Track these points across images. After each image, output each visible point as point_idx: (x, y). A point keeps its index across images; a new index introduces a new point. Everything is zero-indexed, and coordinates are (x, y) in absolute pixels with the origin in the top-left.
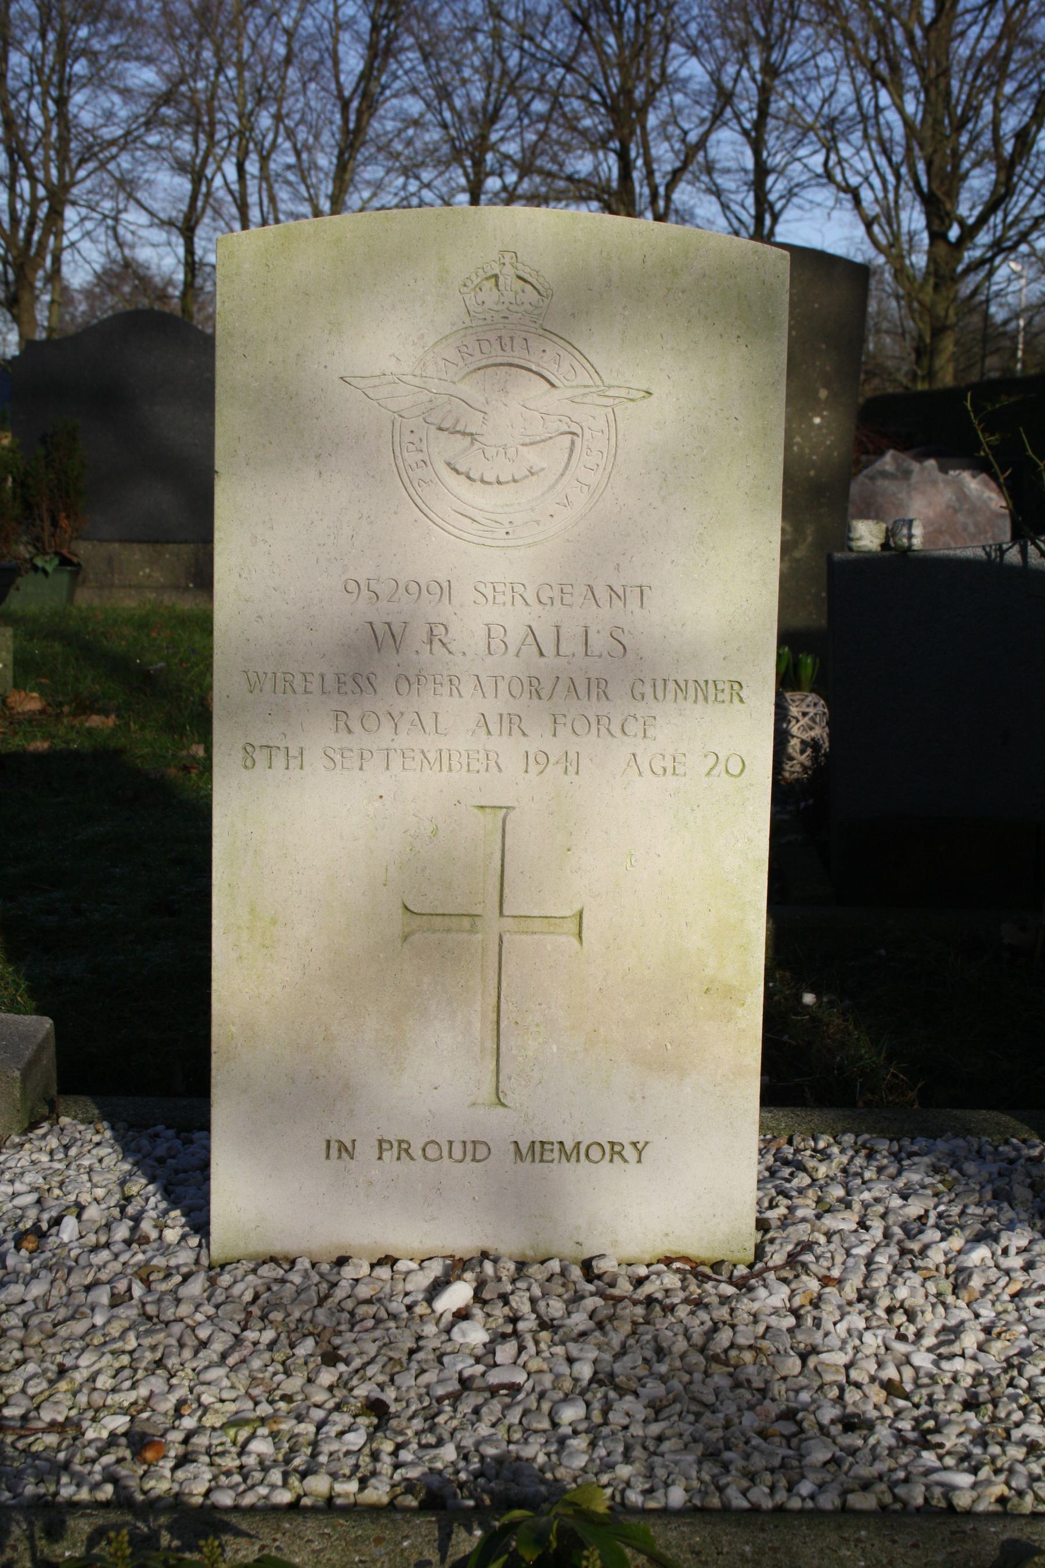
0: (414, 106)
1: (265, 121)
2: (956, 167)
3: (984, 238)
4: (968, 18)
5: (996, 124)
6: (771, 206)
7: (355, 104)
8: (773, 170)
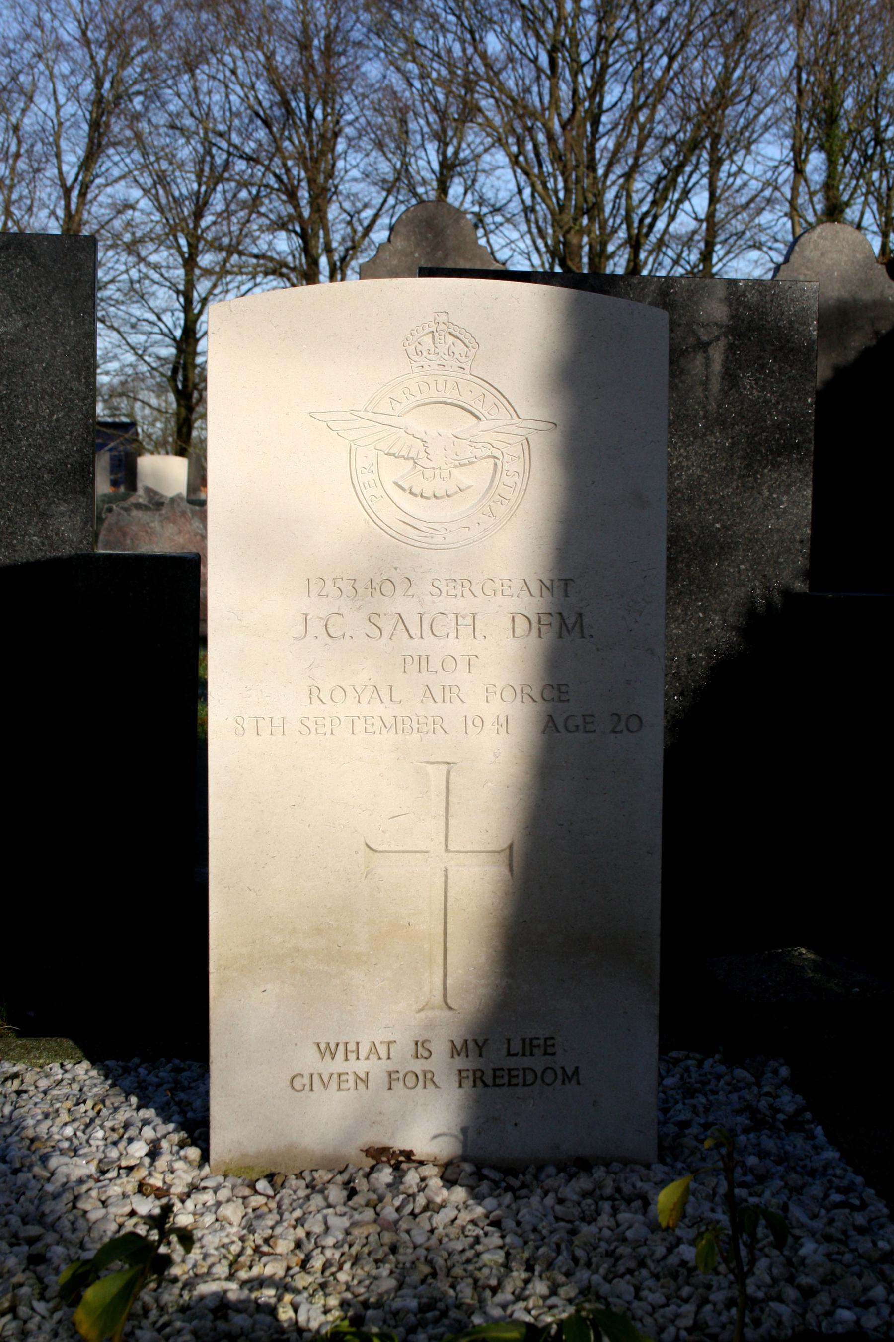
7: (75, 193)
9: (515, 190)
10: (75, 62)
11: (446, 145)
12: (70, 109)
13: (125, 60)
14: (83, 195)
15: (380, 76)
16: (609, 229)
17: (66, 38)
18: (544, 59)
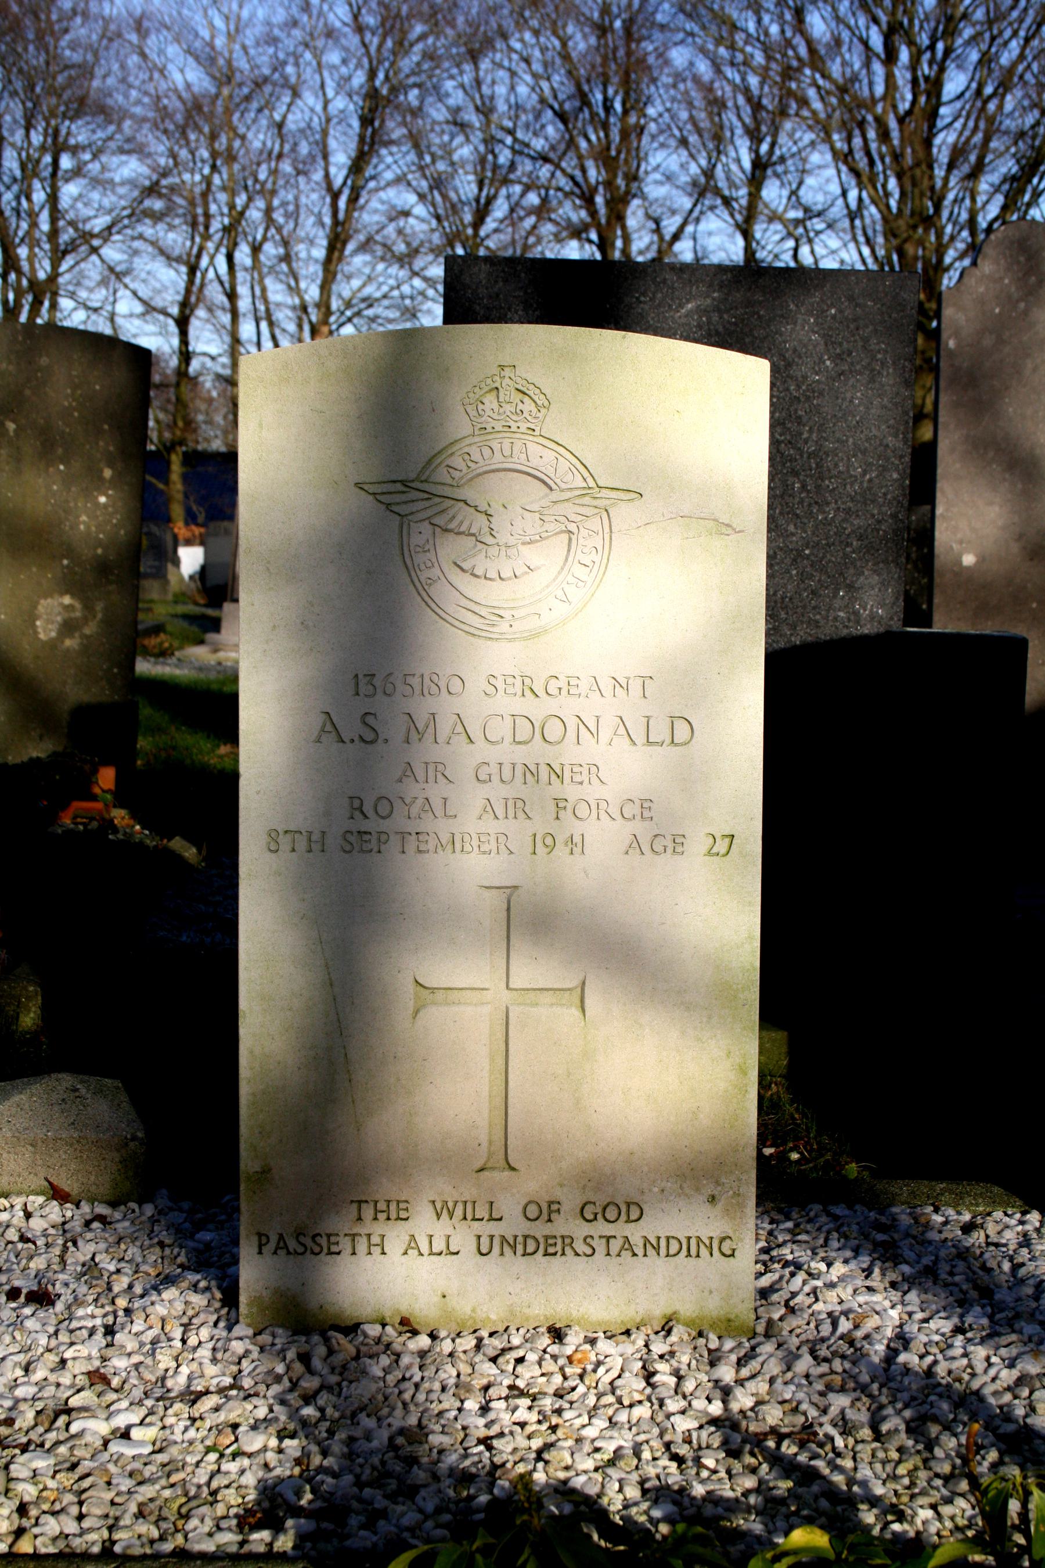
1: (255, 214)
9: (839, 191)
10: (346, 49)
11: (760, 141)
12: (339, 103)
13: (402, 47)
14: (353, 200)
15: (686, 64)
16: (946, 238)
17: (338, 24)
18: (876, 40)
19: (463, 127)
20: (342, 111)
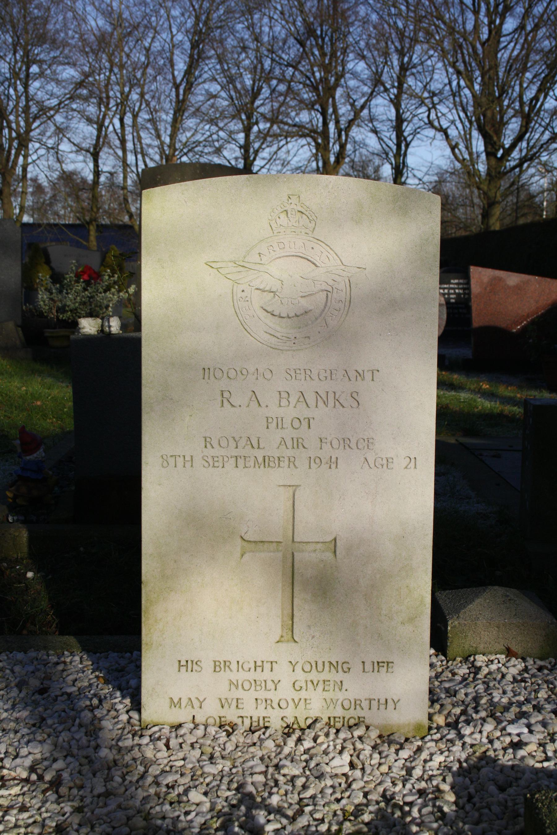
0: (215, 88)
1: (134, 96)
2: (502, 118)
3: (515, 154)
4: (508, 38)
5: (521, 96)
6: (405, 139)
8: (405, 120)
9: (446, 81)
12: (179, 37)
19: (244, 49)
20: (181, 41)
